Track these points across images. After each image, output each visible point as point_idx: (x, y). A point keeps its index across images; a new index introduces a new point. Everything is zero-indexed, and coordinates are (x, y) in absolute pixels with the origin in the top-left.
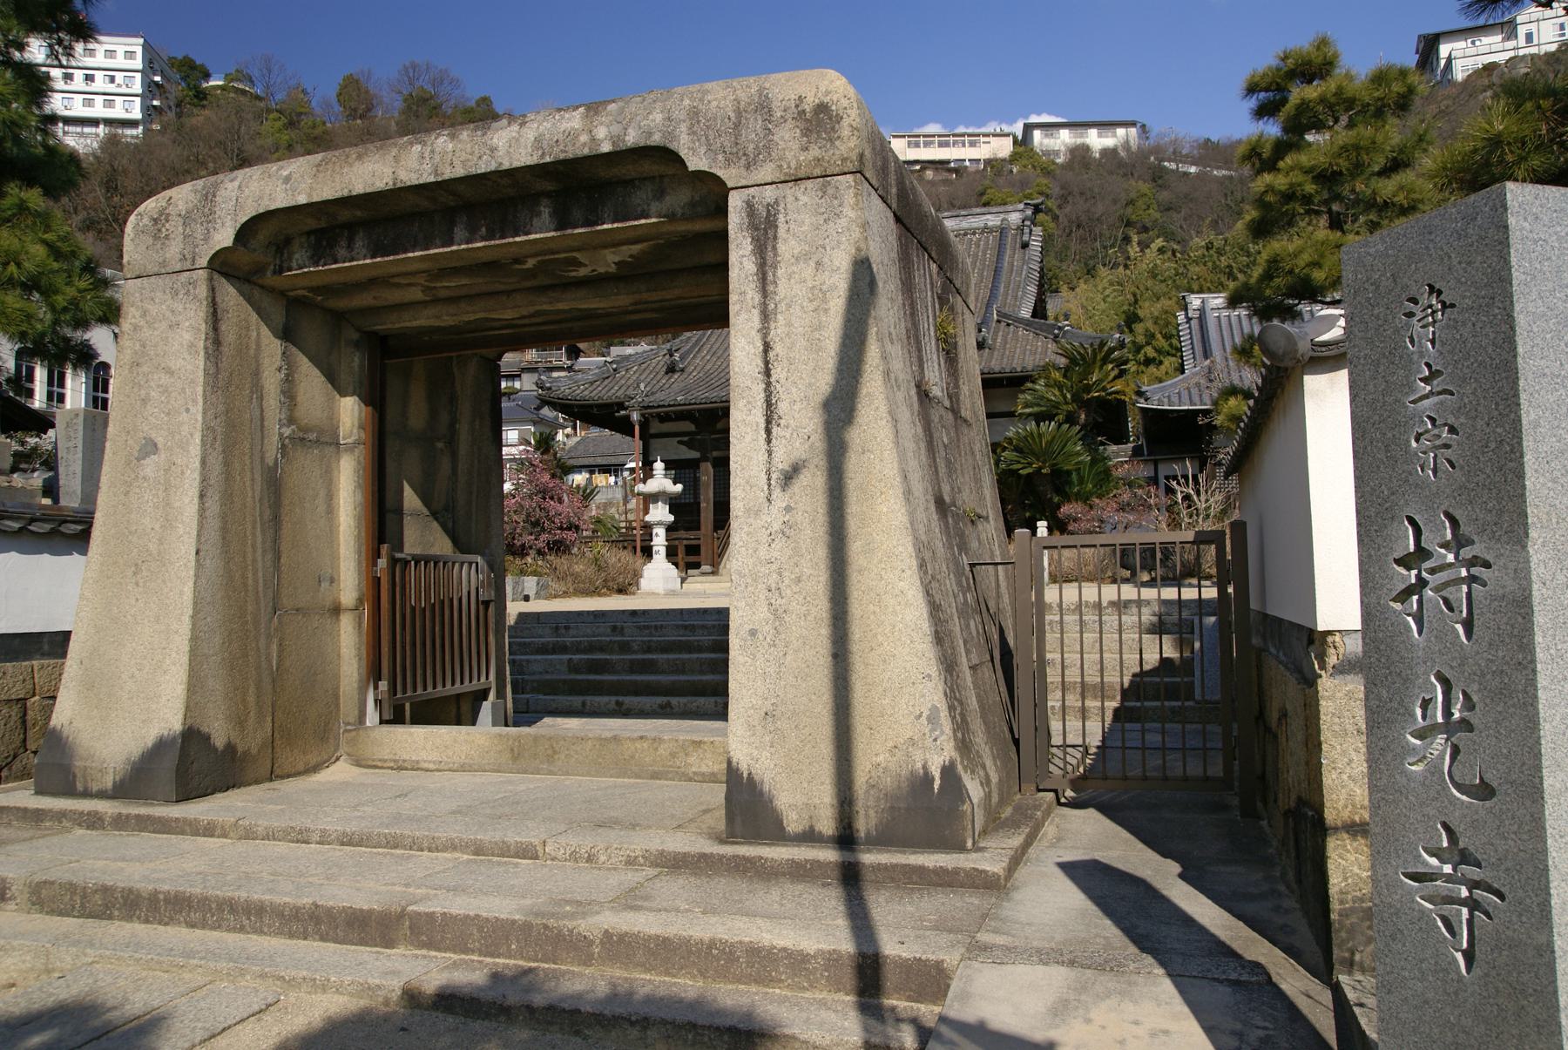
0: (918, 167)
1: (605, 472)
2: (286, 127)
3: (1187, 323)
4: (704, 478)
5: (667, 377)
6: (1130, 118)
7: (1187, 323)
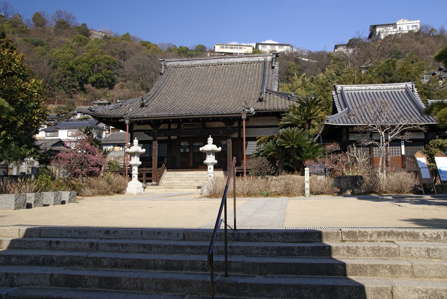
0: (223, 54)
1: (119, 146)
2: (12, 26)
3: (336, 95)
4: (154, 147)
5: (141, 108)
6: (288, 44)
7: (336, 95)
